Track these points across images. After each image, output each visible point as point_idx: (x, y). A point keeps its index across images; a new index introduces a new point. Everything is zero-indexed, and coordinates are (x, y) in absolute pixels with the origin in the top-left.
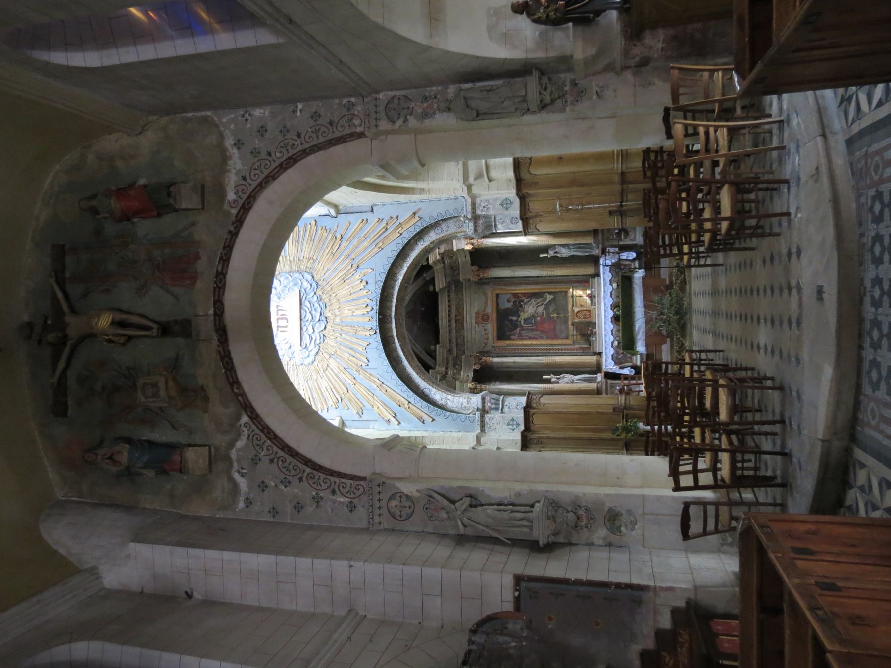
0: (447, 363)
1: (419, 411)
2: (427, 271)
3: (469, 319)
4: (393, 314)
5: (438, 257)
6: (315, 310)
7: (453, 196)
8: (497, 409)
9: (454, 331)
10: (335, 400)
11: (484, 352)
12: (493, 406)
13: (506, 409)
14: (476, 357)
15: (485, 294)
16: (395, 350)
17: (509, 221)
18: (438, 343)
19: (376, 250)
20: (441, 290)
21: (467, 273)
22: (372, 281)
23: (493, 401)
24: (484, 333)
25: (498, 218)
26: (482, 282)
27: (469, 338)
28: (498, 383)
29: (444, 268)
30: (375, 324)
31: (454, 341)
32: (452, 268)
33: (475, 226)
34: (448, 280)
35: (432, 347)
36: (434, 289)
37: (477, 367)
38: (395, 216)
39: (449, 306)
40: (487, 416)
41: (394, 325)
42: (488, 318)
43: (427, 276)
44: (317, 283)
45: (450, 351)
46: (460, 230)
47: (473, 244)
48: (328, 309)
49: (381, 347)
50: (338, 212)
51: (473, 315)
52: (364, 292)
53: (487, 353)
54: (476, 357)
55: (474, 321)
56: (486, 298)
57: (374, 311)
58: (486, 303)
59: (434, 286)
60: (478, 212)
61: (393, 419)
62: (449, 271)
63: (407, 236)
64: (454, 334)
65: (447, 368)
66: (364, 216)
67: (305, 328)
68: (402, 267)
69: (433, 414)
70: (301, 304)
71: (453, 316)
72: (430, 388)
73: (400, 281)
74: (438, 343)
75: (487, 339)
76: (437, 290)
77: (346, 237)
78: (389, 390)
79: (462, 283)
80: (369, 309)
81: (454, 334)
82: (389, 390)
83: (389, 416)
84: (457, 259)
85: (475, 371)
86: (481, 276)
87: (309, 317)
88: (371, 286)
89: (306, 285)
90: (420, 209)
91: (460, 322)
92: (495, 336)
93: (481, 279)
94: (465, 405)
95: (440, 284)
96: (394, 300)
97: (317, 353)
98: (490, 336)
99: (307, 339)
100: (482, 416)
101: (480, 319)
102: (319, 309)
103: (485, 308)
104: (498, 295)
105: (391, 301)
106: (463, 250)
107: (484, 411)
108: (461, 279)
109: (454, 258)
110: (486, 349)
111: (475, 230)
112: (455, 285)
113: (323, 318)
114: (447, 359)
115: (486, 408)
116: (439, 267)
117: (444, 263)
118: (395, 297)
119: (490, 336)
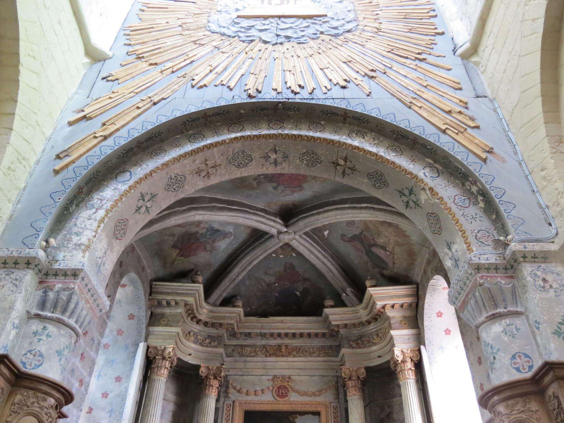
0: (213, 325)
1: (82, 150)
2: (356, 296)
3: (282, 366)
4: (286, 132)
5: (379, 304)
6: (296, 32)
7: (551, 213)
8: (43, 305)
9: (264, 342)
10: (139, 52)
11: (227, 387)
12: (51, 295)
13: (36, 326)
14: (219, 369)
15: (320, 392)
16: (216, 131)
17: (515, 348)
18: (247, 315)
19: (408, 100)
20: (326, 320)
21: (354, 360)
22: (346, 93)
23: (64, 296)
24: (258, 388)
25: (518, 321)
26: (339, 387)
27: (250, 365)
28: (171, 407)
29: (362, 324)
30: (268, 96)
31: (249, 342)
32: (361, 337)
33: (488, 268)
34: (342, 331)
35: (240, 303)
36: (327, 307)
37: (203, 371)
38: (477, 123)
39: (301, 335)
40: (29, 278)
41: (265, 132)
42: (282, 396)
43: (349, 293)
44: (336, 36)
45: (233, 335)
46: (471, 239)
47: (404, 361)
48: (296, 45)
49: (223, 103)
50: (466, 56)
51: (286, 373)
52: (326, 83)
53: (225, 388)
54: (219, 369)
55: (278, 372)
56: (314, 394)
57: (291, 96)
58: (305, 394)
59: (332, 307)
60: (527, 269)
61: (82, 114)
62: (356, 332)
63: (444, 142)
64: (260, 342)
65: (206, 324)
66: (466, 85)
67: (267, 22)
68: (377, 145)
69: (69, 173)
70: (304, 17)
71: (287, 341)
72: (131, 182)
73: (349, 141)
74: (247, 315)
75: (247, 394)
76: (326, 311)
77: (423, 65)
78: (139, 111)
79: (337, 356)
80: (298, 90)
81: (260, 342)
82: (139, 111)
83: (87, 111)
84: (375, 344)
85: (197, 367)
86: (350, 383)
87: (283, 26)
88: (336, 92)
89: (335, 24)
90: (504, 161)
91: (277, 351)
92: (252, 408)
93: (344, 386)
94: (75, 239)
95: (335, 315)
96: (311, 134)
97: (223, 34)
98: (252, 398)
99: (245, 23)
100: (29, 263)
101: (280, 384)
102: (295, 36)
103: (297, 392)
104: (317, 414)
105: (309, 129)
106: (393, 346)
107: (47, 275)
108: (344, 351)
109: (376, 340)
110: (231, 390)
111: (478, 268)
112: (333, 342)
113: (280, 40)
114: (221, 325)
115: (51, 280)
116: (362, 313)
117: (369, 322)
118: (318, 135)
119: (252, 398)
